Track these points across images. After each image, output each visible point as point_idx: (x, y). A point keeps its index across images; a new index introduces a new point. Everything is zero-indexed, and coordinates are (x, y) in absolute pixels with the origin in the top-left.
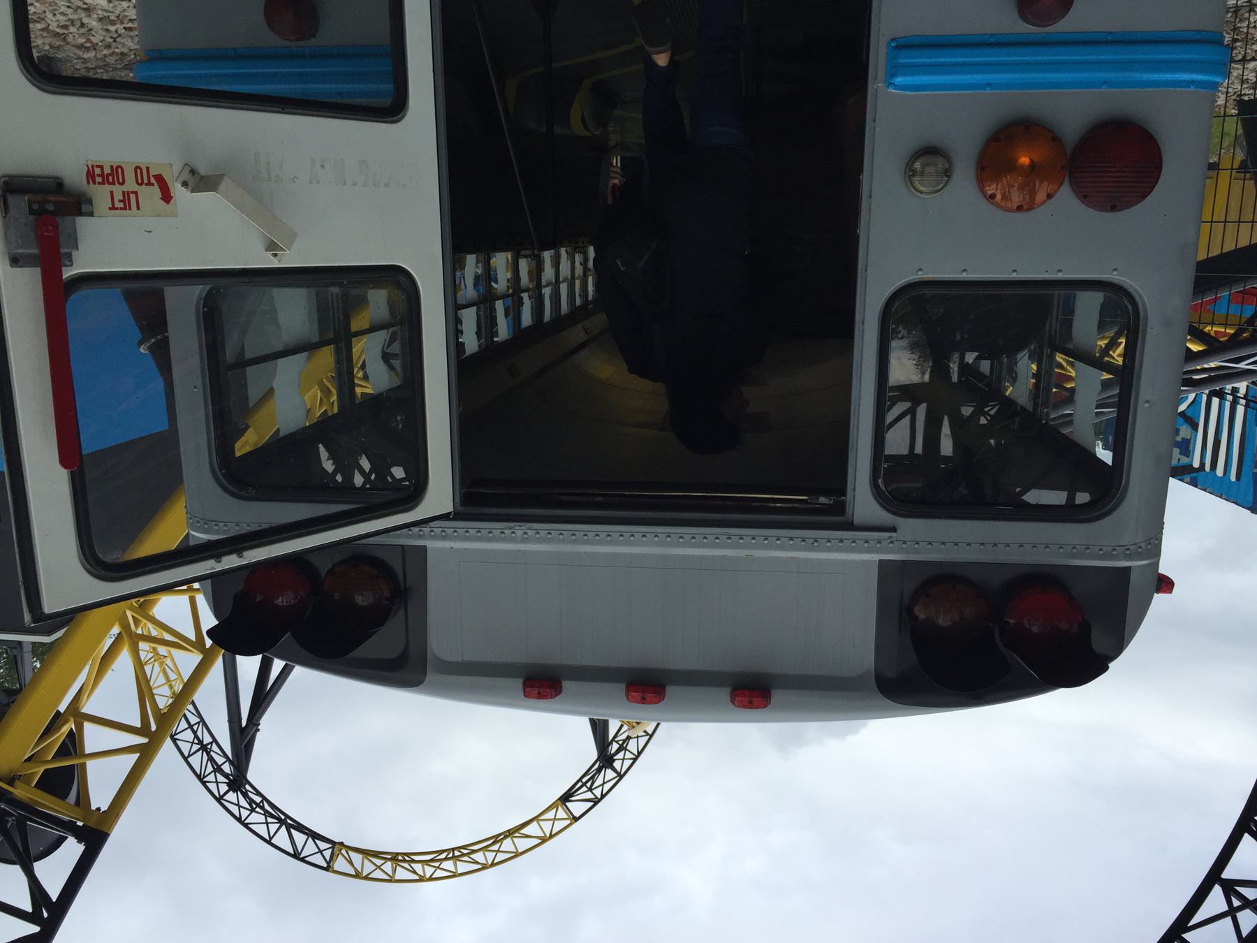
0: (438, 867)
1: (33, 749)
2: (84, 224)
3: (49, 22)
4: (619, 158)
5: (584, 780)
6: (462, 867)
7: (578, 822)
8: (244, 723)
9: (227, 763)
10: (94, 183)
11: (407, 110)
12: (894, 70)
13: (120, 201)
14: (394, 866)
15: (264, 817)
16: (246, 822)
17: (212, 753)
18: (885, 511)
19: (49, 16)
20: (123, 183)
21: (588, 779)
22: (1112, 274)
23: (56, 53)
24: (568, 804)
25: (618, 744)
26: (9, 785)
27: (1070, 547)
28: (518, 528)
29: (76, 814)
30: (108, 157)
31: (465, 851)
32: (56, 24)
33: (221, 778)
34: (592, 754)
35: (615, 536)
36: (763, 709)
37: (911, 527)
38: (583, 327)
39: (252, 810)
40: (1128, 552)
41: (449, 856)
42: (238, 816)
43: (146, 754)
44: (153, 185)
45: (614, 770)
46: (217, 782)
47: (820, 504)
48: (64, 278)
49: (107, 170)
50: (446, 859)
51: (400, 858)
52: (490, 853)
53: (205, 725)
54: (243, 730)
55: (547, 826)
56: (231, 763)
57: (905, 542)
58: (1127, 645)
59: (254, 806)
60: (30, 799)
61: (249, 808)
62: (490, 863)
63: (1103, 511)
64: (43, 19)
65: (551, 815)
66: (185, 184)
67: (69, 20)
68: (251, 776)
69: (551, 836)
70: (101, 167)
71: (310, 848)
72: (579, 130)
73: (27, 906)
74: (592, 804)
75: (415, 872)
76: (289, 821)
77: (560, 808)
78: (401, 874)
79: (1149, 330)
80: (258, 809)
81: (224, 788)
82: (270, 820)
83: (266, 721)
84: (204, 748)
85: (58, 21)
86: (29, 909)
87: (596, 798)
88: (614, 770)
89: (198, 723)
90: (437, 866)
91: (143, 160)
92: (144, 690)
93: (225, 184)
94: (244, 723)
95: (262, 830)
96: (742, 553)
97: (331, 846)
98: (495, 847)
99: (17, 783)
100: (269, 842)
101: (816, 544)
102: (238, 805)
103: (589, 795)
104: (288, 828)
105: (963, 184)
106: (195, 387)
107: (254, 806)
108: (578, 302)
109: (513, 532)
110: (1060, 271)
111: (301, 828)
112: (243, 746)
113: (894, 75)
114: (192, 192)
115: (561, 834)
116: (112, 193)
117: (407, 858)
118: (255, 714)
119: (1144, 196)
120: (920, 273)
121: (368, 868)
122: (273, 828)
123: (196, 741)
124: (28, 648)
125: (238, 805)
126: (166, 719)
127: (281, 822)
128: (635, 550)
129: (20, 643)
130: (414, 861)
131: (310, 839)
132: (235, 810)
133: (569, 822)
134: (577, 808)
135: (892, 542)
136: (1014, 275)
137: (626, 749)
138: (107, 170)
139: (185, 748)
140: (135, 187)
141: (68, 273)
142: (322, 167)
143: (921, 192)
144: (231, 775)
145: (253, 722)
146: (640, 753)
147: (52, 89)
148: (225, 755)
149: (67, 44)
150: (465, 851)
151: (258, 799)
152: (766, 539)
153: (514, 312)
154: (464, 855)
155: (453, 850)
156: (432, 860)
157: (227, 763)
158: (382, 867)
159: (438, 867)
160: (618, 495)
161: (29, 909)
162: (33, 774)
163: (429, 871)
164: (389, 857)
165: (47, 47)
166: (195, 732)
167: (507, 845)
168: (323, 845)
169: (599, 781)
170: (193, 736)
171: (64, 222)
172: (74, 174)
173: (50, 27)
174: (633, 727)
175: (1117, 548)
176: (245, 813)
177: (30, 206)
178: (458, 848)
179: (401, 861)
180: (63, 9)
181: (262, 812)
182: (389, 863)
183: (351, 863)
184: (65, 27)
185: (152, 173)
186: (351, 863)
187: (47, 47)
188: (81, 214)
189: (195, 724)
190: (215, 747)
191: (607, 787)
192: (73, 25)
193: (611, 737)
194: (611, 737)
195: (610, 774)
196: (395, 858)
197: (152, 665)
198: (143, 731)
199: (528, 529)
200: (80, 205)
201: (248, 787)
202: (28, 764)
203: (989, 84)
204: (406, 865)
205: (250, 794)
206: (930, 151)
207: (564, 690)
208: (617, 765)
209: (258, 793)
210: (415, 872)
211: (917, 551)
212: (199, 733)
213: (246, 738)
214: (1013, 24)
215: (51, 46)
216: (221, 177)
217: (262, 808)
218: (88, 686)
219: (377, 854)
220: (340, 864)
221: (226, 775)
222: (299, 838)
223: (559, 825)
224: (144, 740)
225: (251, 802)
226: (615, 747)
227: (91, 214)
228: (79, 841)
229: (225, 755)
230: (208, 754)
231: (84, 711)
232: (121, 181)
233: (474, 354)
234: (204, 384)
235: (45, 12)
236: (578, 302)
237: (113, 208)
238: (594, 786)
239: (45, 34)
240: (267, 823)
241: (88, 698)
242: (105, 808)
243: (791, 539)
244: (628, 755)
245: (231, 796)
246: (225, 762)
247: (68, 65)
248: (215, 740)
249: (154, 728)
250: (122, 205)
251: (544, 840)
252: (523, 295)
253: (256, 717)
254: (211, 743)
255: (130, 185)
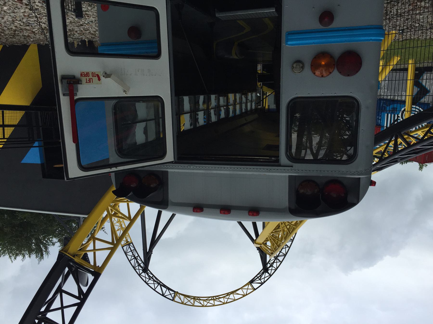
0: (208, 302)
1: (80, 248)
2: (80, 86)
3: (90, 30)
4: (262, 65)
5: (258, 276)
6: (216, 303)
7: (256, 290)
8: (148, 251)
9: (142, 263)
10: (82, 76)
11: (161, 56)
12: (287, 40)
13: (88, 81)
14: (194, 301)
15: (153, 282)
16: (147, 283)
17: (138, 260)
18: (288, 161)
19: (91, 29)
20: (89, 77)
21: (259, 276)
22: (350, 94)
23: (93, 39)
24: (252, 284)
25: (270, 264)
26: (73, 257)
27: (338, 172)
28: (192, 166)
29: (92, 267)
30: (85, 70)
31: (217, 298)
32: (92, 31)
33: (140, 268)
34: (261, 267)
35: (217, 168)
36: (255, 217)
37: (297, 166)
38: (245, 119)
39: (150, 279)
40: (359, 173)
41: (212, 299)
42: (145, 281)
43: (113, 250)
44: (96, 77)
45: (268, 273)
46: (139, 269)
47: (273, 160)
48: (75, 99)
49: (85, 74)
50: (211, 300)
51: (196, 298)
52: (225, 299)
53: (136, 250)
54: (147, 253)
55: (245, 291)
56: (143, 263)
57: (295, 170)
58: (360, 202)
59: (150, 278)
60: (79, 262)
61: (149, 278)
62: (226, 302)
63: (352, 161)
64: (89, 30)
65: (246, 287)
66: (104, 76)
67: (96, 30)
68: (149, 268)
69: (247, 295)
70: (84, 73)
71: (167, 293)
72: (235, 57)
73: (77, 294)
74: (260, 284)
75: (201, 303)
76: (161, 284)
77: (249, 285)
78: (196, 304)
79: (362, 110)
80: (151, 279)
81: (141, 271)
82: (155, 283)
83: (155, 251)
84: (135, 258)
85: (93, 30)
86: (78, 295)
87: (262, 282)
88: (268, 273)
89: (134, 250)
90: (208, 302)
91: (93, 71)
92: (113, 231)
93: (112, 76)
94: (148, 251)
95: (152, 286)
96: (251, 173)
97: (174, 293)
98: (228, 297)
99: (76, 256)
100: (155, 290)
101: (271, 171)
102: (145, 277)
103: (259, 281)
104: (161, 286)
105: (307, 70)
106: (112, 129)
107: (150, 278)
108: (243, 111)
109: (190, 167)
110: (335, 93)
111: (165, 286)
112: (147, 258)
113: (287, 42)
114: (105, 78)
115: (249, 295)
116: (86, 79)
117: (198, 299)
118: (152, 247)
119: (357, 72)
120: (297, 95)
121: (186, 301)
122: (156, 285)
123: (133, 256)
124: (82, 220)
125: (145, 277)
126: (119, 240)
127: (159, 284)
128: (222, 172)
129: (79, 218)
130: (200, 300)
131: (167, 290)
132: (144, 279)
133: (252, 290)
134: (255, 285)
135: (291, 170)
136: (323, 95)
137: (272, 266)
138: (85, 74)
139: (130, 258)
140: (92, 77)
141: (76, 98)
142: (138, 71)
143: (296, 73)
144: (143, 267)
145: (151, 250)
146: (277, 268)
147: (72, 55)
148: (142, 261)
149: (96, 37)
150: (217, 298)
151: (151, 276)
152: (257, 169)
153: (218, 113)
154: (217, 299)
155: (213, 297)
156: (206, 300)
157: (142, 263)
158: (190, 301)
159: (208, 302)
160: (218, 157)
161: (78, 295)
162: (81, 254)
163: (205, 303)
164: (193, 298)
165: (90, 38)
166: (133, 253)
167: (231, 296)
168: (171, 292)
169: (263, 277)
170: (132, 254)
171: (75, 86)
172: (77, 74)
173: (91, 32)
174: (271, 255)
175: (356, 172)
176: (147, 280)
177: (67, 82)
178: (215, 296)
179: (196, 299)
180: (94, 27)
181: (153, 280)
182: (192, 300)
183: (180, 299)
184: (95, 32)
185: (96, 74)
186: (180, 299)
187: (90, 38)
188: (79, 84)
189: (133, 250)
190: (139, 258)
191: (266, 279)
192: (97, 31)
193: (267, 261)
194: (267, 261)
195: (267, 274)
196: (194, 298)
197: (120, 231)
198: (112, 243)
199: (194, 166)
200: (79, 81)
201: (148, 272)
202: (80, 251)
203: (314, 43)
204: (198, 301)
205: (149, 274)
206: (298, 62)
207: (204, 211)
208: (269, 271)
209: (152, 274)
210: (201, 303)
211: (298, 173)
212: (134, 253)
213: (148, 255)
214: (318, 26)
215: (92, 37)
216: (111, 74)
217: (153, 279)
218: (97, 230)
219: (189, 296)
220: (177, 299)
221: (142, 267)
222: (164, 289)
223: (249, 291)
224: (112, 246)
225: (149, 276)
226: (269, 265)
227: (81, 84)
228: (93, 276)
229: (142, 261)
230: (137, 260)
231: (96, 237)
232: (88, 76)
233: (202, 125)
234: (114, 128)
235: (89, 28)
236: (243, 111)
237: (87, 82)
238: (261, 279)
239: (89, 34)
240: (154, 284)
241: (97, 233)
242: (100, 266)
243: (264, 169)
244: (273, 268)
245: (143, 274)
246: (141, 263)
247: (96, 43)
248: (139, 256)
249: (115, 242)
250: (89, 82)
251: (244, 296)
252: (221, 108)
253: (151, 249)
254: (137, 256)
255: (91, 77)
